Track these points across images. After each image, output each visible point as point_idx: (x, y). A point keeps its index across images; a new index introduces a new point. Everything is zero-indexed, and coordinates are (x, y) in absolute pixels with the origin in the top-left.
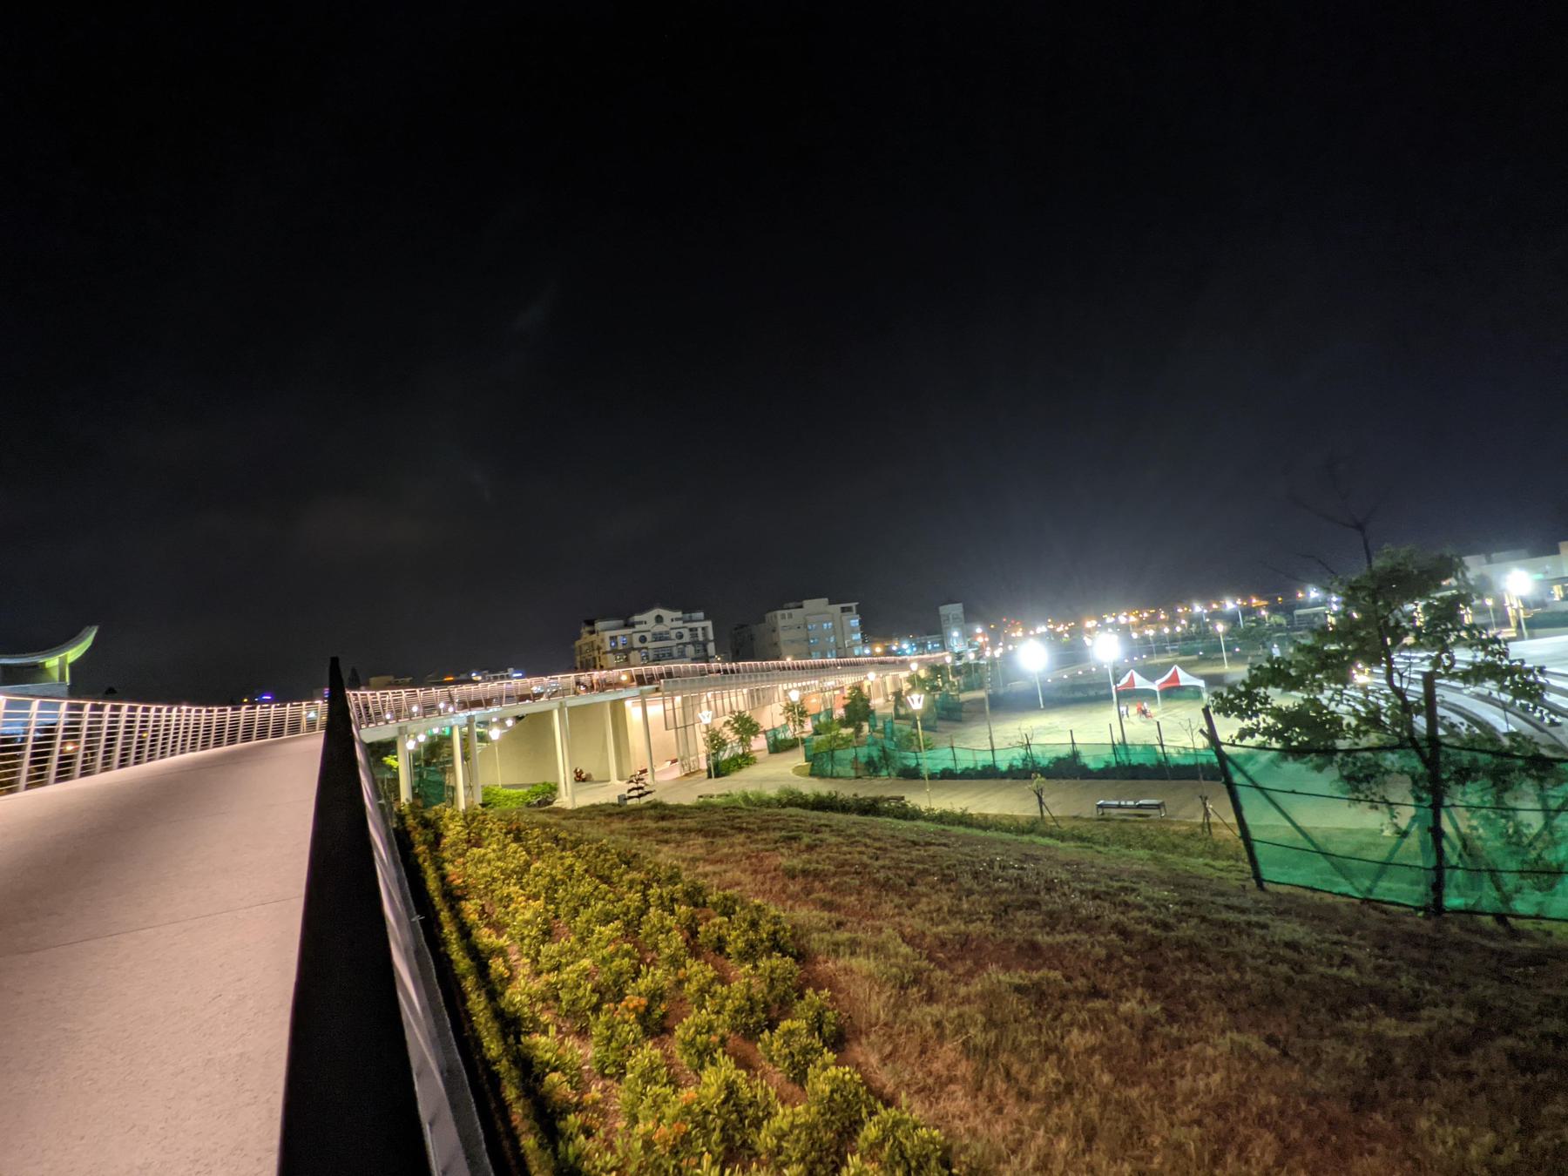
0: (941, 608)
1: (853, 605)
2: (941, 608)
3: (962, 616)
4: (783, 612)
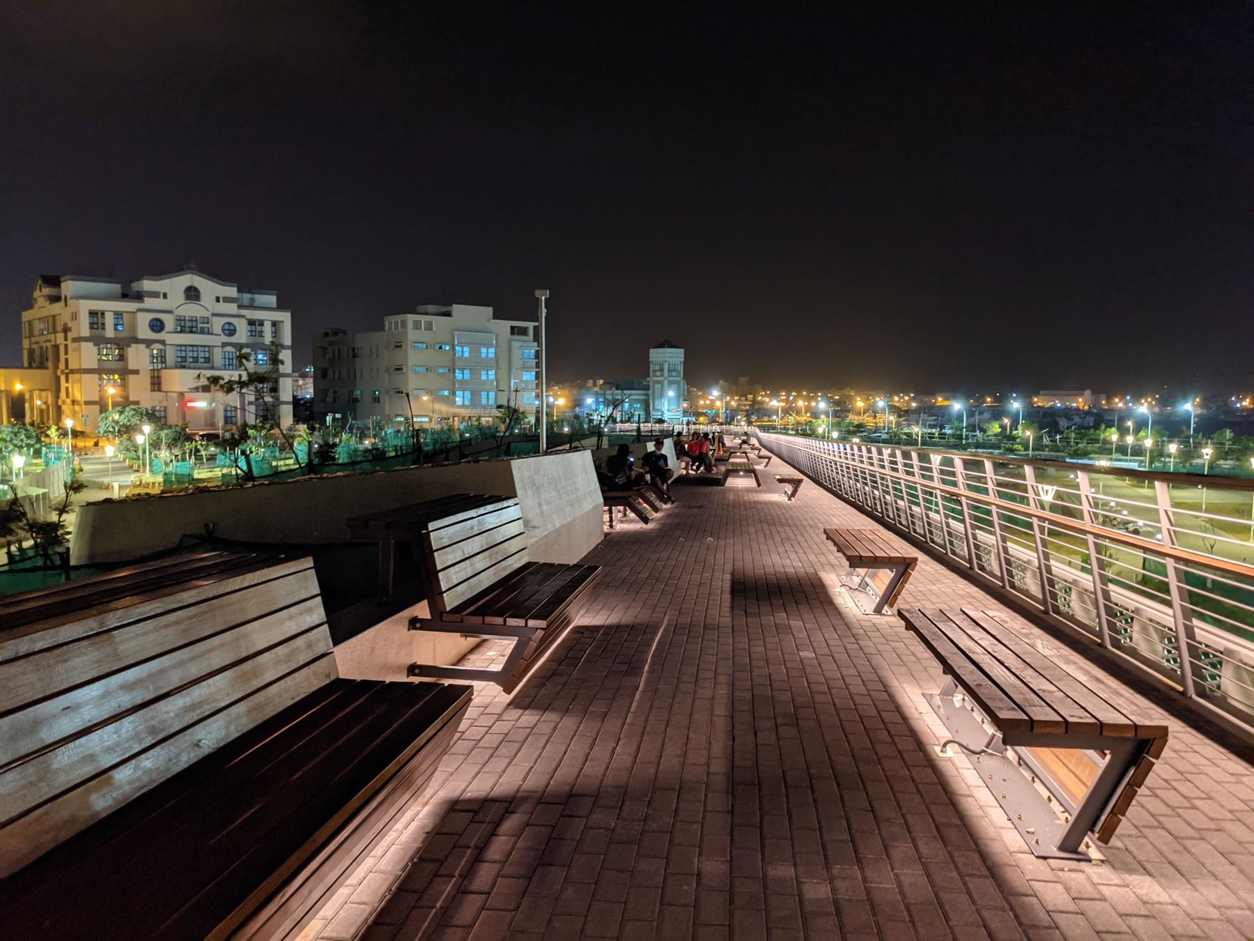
0: (653, 351)
3: (681, 368)
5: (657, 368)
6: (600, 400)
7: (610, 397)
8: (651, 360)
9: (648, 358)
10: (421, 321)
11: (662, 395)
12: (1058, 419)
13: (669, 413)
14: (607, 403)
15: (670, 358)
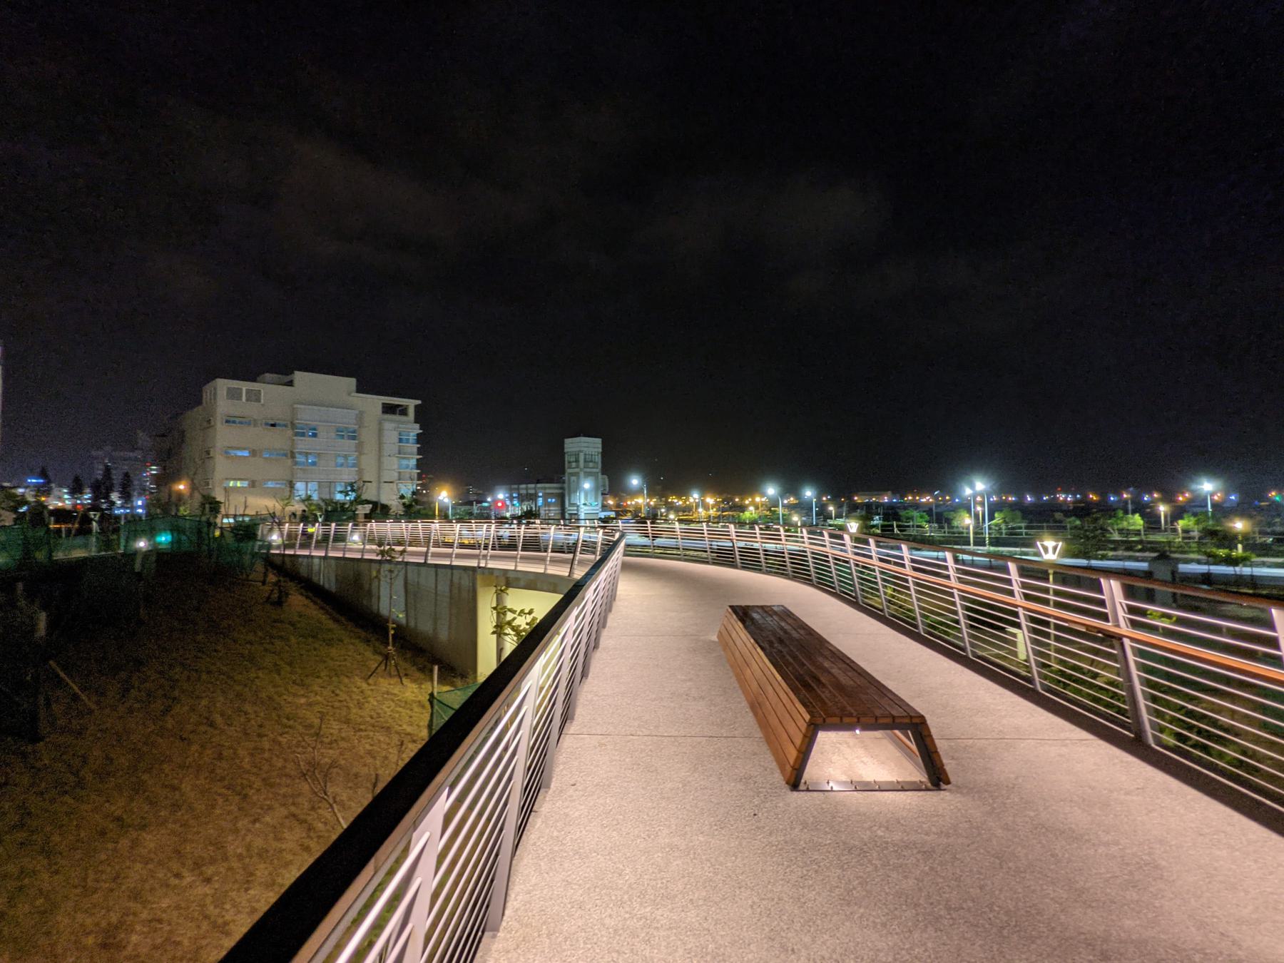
0: (568, 441)
1: (411, 404)
2: (568, 441)
3: (598, 459)
4: (235, 384)
5: (573, 459)
6: (514, 495)
7: (523, 492)
8: (566, 450)
9: (563, 449)
10: (241, 389)
11: (578, 487)
12: (898, 510)
13: (586, 508)
14: (522, 499)
15: (586, 448)
